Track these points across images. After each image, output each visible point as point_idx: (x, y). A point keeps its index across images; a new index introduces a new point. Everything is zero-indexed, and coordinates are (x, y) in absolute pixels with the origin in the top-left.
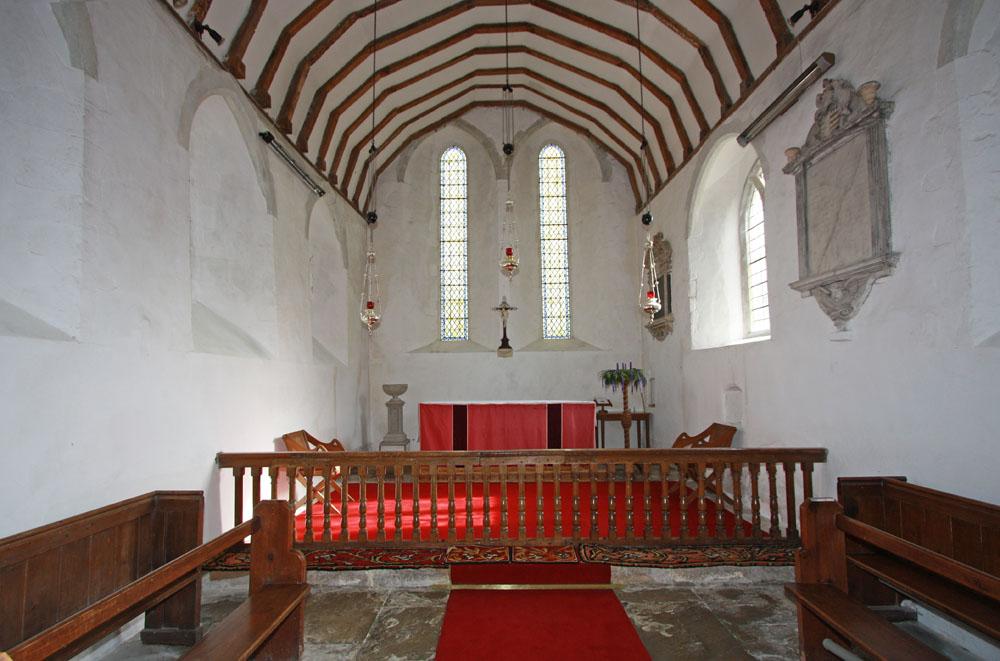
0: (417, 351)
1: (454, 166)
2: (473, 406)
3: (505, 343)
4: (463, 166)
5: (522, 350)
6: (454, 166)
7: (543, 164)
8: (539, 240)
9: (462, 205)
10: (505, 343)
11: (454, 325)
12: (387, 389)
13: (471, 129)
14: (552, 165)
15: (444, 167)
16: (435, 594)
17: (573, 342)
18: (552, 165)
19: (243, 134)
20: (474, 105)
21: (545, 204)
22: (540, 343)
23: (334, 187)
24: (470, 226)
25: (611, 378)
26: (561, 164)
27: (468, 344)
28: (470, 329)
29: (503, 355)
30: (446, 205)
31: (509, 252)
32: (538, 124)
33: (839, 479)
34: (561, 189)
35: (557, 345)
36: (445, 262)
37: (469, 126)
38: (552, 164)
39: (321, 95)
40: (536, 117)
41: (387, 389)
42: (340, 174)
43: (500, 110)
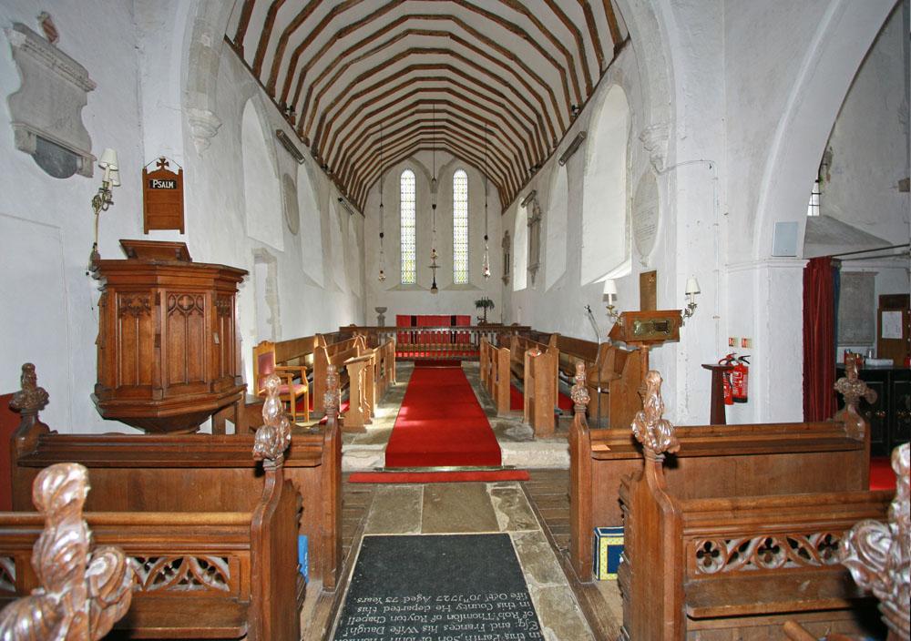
0: (389, 290)
1: (408, 181)
2: (419, 316)
3: (434, 286)
4: (413, 182)
5: (446, 289)
6: (408, 181)
7: (456, 181)
8: (452, 227)
9: (413, 205)
10: (434, 286)
11: (408, 274)
12: (378, 310)
13: (418, 163)
14: (460, 180)
15: (403, 182)
16: (409, 369)
17: (469, 286)
18: (460, 180)
19: (292, 154)
20: (419, 149)
21: (456, 205)
22: (453, 286)
23: (273, 101)
24: (417, 218)
25: (479, 304)
26: (466, 182)
27: (416, 287)
28: (417, 278)
29: (433, 292)
30: (403, 205)
31: (434, 251)
32: (453, 161)
33: (469, 317)
34: (465, 197)
35: (461, 287)
36: (403, 239)
37: (418, 162)
38: (460, 182)
39: (311, 89)
40: (452, 157)
41: (378, 310)
42: (289, 103)
43: (432, 152)
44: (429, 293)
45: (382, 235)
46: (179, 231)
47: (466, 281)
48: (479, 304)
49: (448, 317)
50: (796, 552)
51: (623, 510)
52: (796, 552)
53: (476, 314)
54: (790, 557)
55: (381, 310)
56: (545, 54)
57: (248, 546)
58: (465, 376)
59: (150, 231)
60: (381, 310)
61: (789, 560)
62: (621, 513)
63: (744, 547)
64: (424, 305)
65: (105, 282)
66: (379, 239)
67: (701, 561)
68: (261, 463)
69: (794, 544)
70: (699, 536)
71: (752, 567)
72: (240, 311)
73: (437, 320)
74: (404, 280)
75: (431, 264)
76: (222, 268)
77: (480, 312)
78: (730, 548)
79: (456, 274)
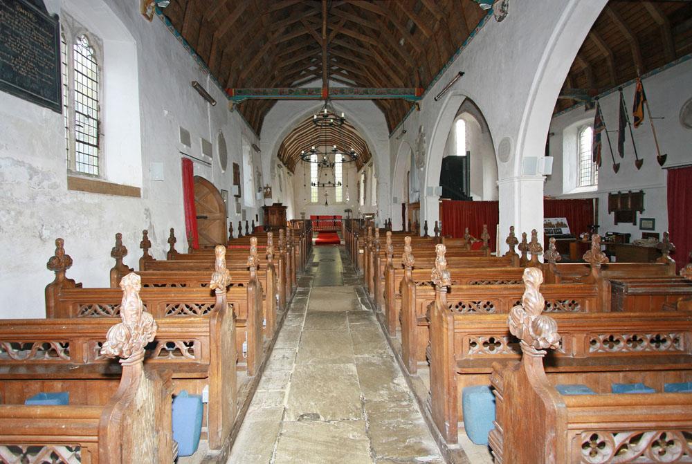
6: (587, 302)
12: (301, 213)
17: (344, 203)
22: (335, 203)
25: (346, 211)
27: (319, 203)
41: (301, 213)
46: (631, 224)
48: (346, 211)
51: (494, 395)
53: (344, 215)
54: (686, 451)
55: (303, 214)
57: (95, 438)
59: (619, 223)
60: (303, 214)
61: (685, 454)
62: (492, 398)
63: (635, 440)
67: (587, 451)
68: (214, 290)
71: (645, 459)
73: (328, 217)
74: (312, 201)
78: (619, 439)
79: (312, 199)
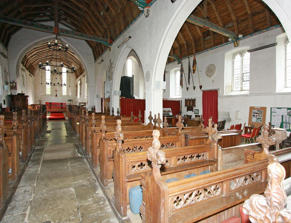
10: (56, 95)
25: (69, 101)
43: (287, 81)
44: (55, 97)
45: (42, 84)
47: (66, 95)
48: (69, 101)
49: (60, 103)
50: (207, 193)
52: (207, 193)
56: (156, 69)
58: (46, 116)
63: (190, 195)
64: (54, 100)
65: (245, 195)
66: (41, 84)
69: (206, 190)
70: (175, 196)
72: (284, 174)
75: (57, 92)
76: (121, 101)
77: (69, 102)
